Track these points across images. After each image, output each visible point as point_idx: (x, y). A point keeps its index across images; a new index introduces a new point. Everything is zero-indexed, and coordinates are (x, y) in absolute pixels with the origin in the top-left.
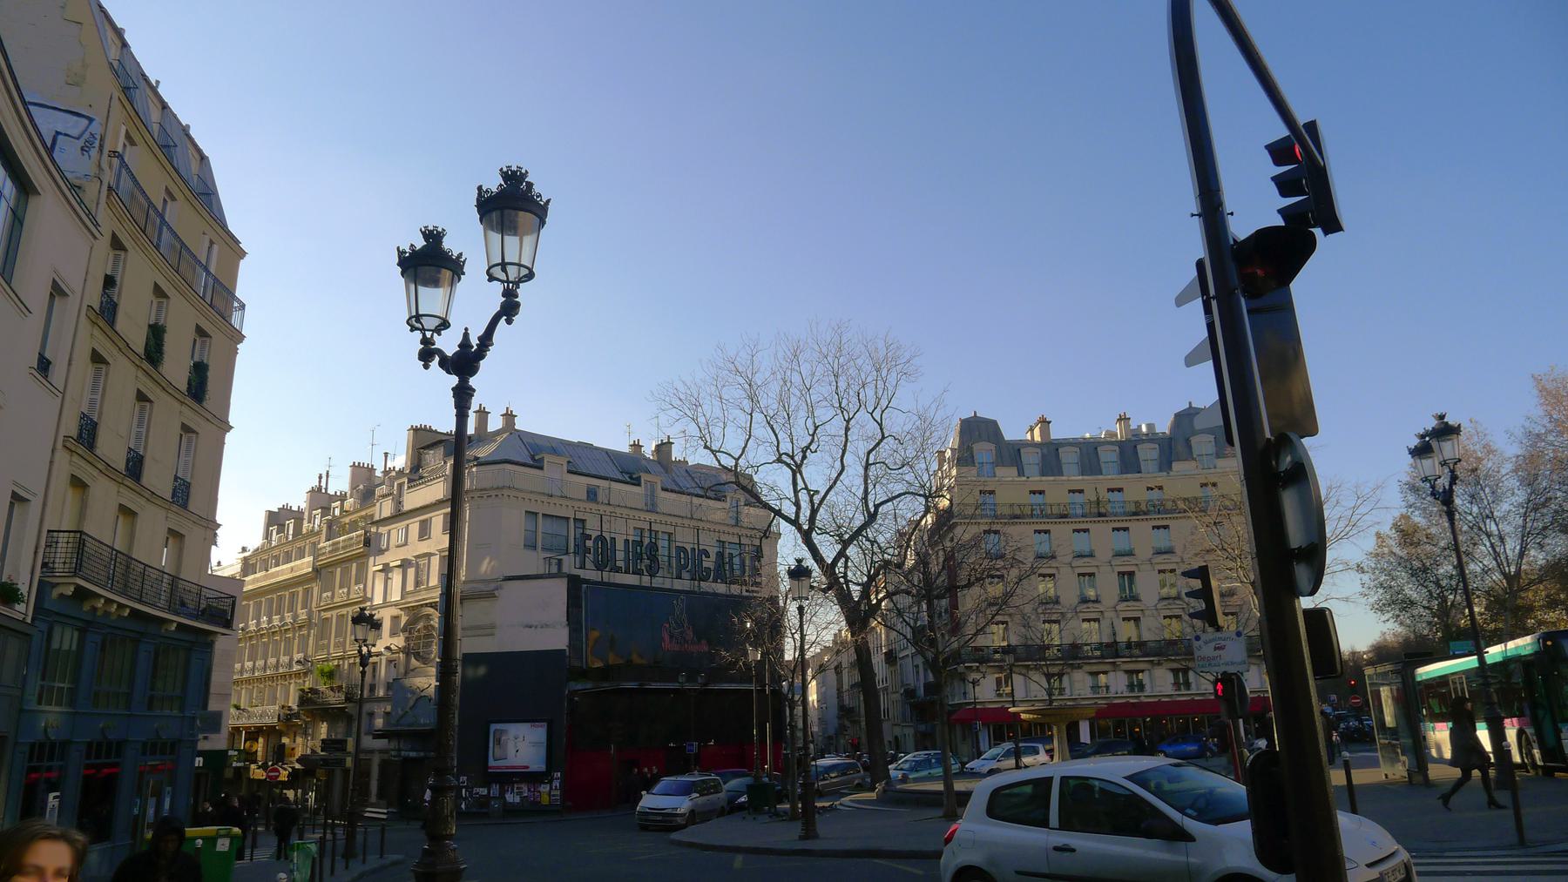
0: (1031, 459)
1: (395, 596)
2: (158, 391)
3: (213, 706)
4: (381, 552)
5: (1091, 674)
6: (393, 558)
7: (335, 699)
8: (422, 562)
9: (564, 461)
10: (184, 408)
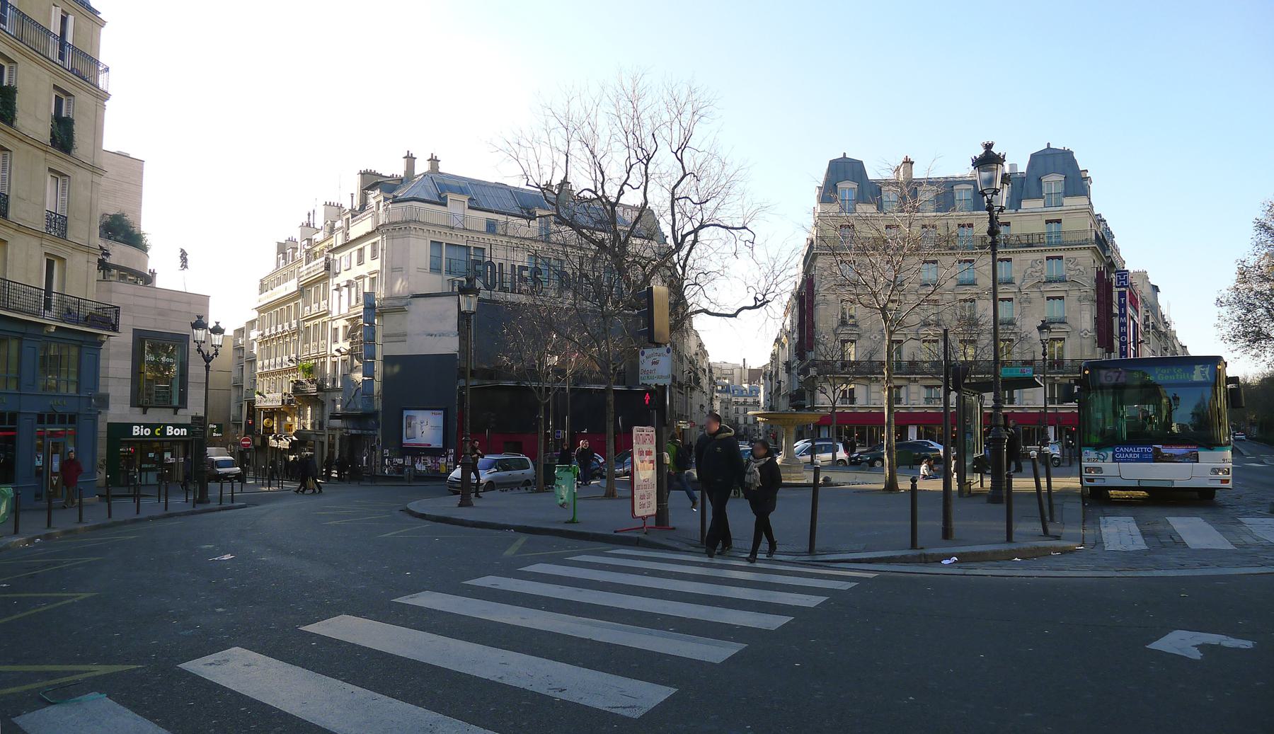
0: (890, 195)
1: (344, 310)
2: (15, 142)
3: (102, 390)
4: (336, 274)
5: (926, 387)
6: (341, 279)
7: (312, 389)
8: (360, 282)
9: (465, 199)
10: (48, 156)
